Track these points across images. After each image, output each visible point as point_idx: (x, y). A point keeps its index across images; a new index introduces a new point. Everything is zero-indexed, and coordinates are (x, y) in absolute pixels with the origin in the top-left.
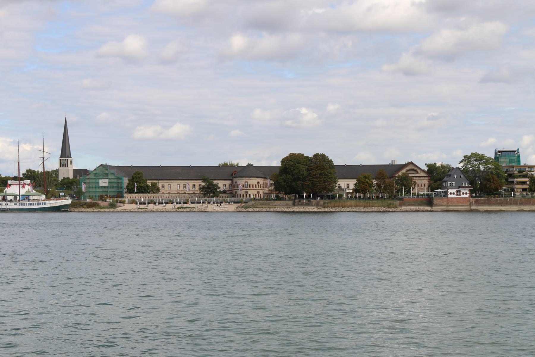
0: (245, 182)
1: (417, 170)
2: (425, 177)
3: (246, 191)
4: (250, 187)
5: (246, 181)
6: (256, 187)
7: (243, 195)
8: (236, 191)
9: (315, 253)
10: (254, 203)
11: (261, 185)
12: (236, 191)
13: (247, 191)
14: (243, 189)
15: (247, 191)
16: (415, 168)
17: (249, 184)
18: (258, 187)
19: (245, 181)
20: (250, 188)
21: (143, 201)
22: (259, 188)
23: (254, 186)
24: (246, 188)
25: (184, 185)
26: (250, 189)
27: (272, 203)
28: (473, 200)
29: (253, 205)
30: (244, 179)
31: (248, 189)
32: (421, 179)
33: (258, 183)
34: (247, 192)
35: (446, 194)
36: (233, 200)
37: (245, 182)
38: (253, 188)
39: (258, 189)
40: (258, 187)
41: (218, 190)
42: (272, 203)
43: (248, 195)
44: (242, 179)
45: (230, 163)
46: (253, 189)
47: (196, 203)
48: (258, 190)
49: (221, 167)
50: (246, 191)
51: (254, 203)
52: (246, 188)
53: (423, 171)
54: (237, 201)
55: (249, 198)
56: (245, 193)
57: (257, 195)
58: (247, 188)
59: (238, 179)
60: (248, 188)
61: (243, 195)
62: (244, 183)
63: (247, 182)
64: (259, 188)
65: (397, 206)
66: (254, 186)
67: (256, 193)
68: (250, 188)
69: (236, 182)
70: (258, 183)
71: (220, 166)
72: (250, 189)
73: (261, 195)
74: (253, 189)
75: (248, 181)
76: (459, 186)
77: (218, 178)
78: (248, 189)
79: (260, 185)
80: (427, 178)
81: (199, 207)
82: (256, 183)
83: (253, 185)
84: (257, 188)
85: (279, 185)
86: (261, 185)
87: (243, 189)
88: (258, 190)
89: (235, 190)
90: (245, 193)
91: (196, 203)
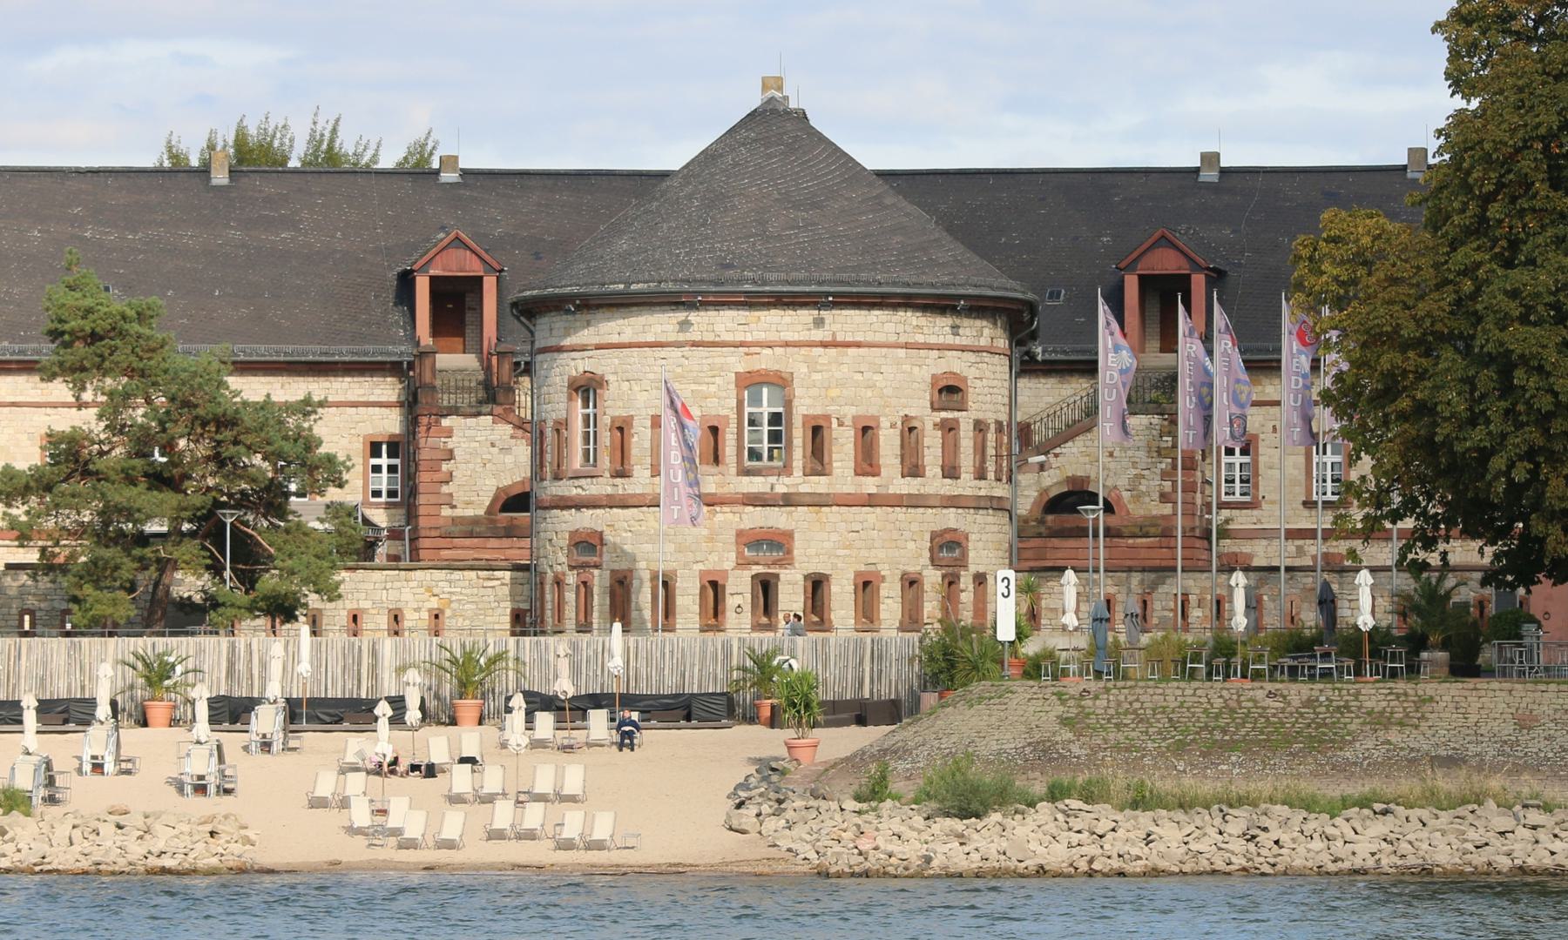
0: (750, 382)
5: (766, 361)
6: (867, 462)
7: (714, 589)
8: (586, 520)
10: (1064, 721)
11: (991, 436)
12: (586, 520)
13: (777, 519)
15: (777, 519)
17: (805, 406)
18: (951, 472)
19: (737, 362)
20: (819, 485)
22: (967, 475)
23: (888, 443)
24: (757, 485)
26: (818, 502)
27: (1380, 721)
29: (1044, 753)
31: (788, 501)
34: (777, 544)
36: (616, 663)
37: (750, 382)
38: (870, 485)
39: (948, 488)
40: (913, 469)
41: (309, 511)
42: (1380, 721)
43: (791, 598)
45: (316, 143)
46: (871, 501)
47: (30, 718)
48: (951, 519)
49: (220, 177)
51: (1064, 721)
52: (757, 485)
53: (454, 411)
54: (669, 686)
56: (742, 564)
57: (932, 578)
58: (782, 486)
60: (798, 482)
61: (714, 589)
63: (781, 382)
64: (967, 475)
66: (888, 443)
67: (915, 556)
68: (819, 485)
69: (587, 388)
70: (950, 392)
71: (204, 171)
74: (871, 501)
75: (795, 364)
76: (1305, 504)
78: (788, 501)
79: (980, 427)
81: (84, 794)
82: (919, 405)
83: (866, 431)
84: (933, 483)
85: (1496, 408)
86: (991, 436)
88: (951, 519)
89: (578, 505)
90: (742, 564)
91: (30, 718)
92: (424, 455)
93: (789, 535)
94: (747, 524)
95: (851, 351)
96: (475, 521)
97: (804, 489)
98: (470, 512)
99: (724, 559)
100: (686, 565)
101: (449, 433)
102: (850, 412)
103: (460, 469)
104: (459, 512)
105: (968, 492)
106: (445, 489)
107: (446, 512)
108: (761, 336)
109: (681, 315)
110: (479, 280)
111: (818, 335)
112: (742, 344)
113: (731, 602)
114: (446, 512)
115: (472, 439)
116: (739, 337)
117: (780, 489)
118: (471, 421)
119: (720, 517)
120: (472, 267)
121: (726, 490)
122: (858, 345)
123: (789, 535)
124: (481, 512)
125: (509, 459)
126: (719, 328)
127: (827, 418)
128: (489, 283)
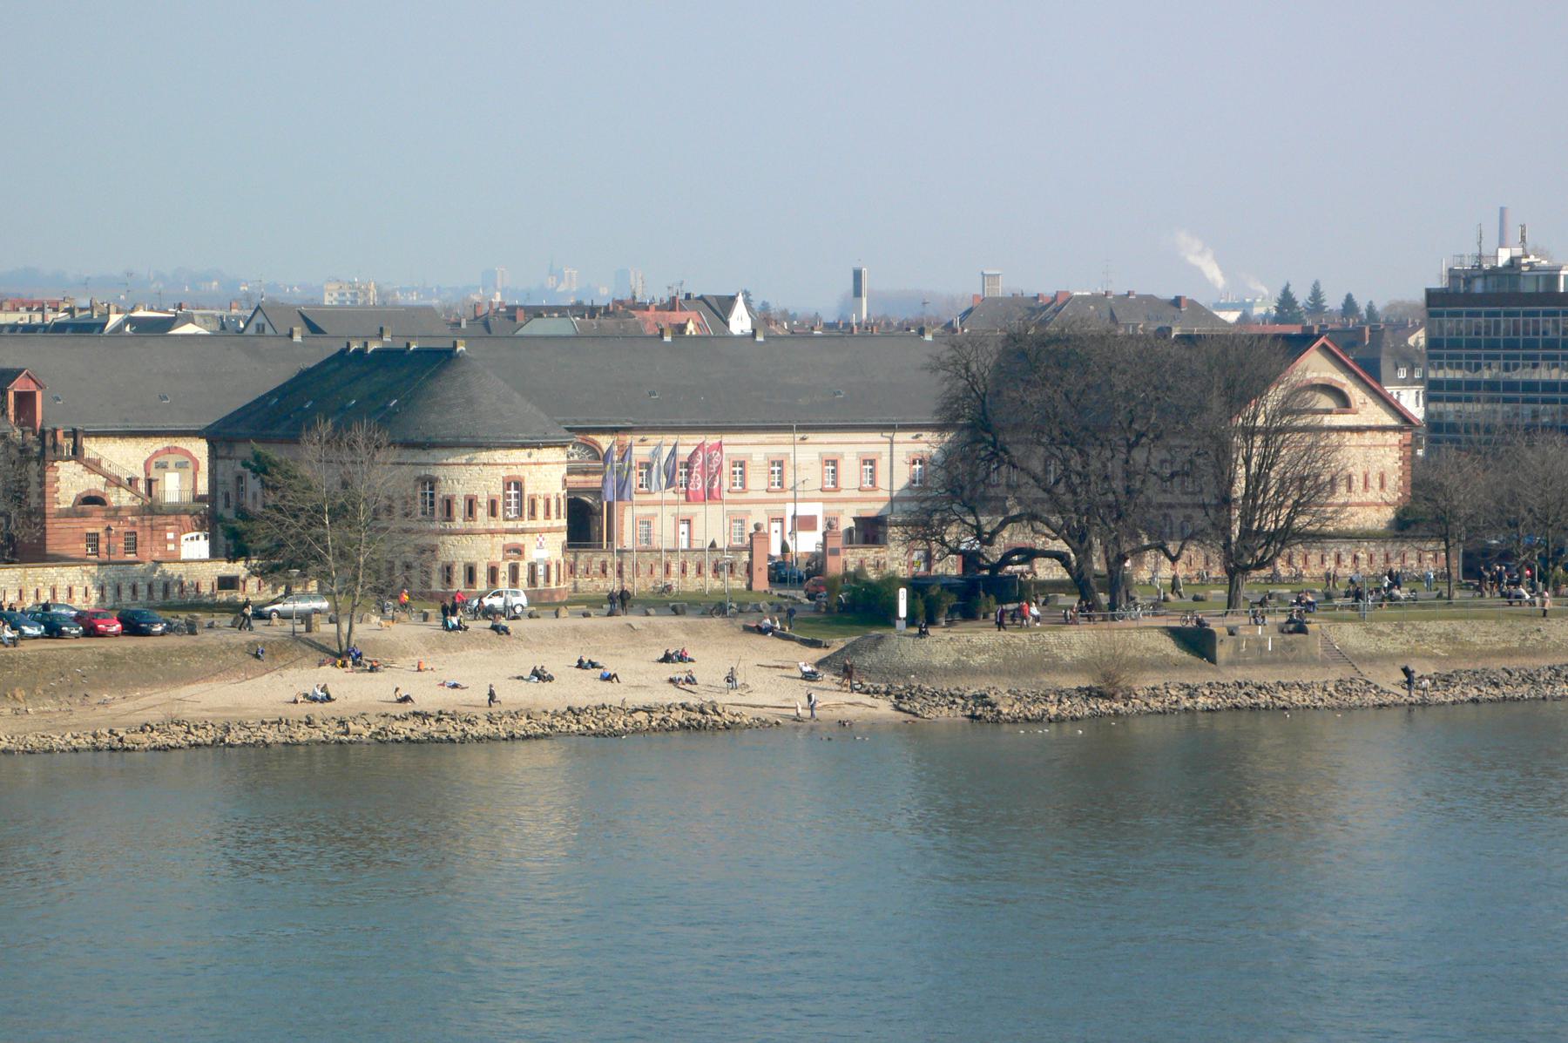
1: (1346, 390)
2: (1384, 429)
3: (511, 539)
4: (449, 514)
5: (514, 472)
9: (1081, 903)
13: (519, 539)
14: (492, 532)
15: (519, 539)
16: (1334, 377)
17: (529, 490)
19: (503, 472)
21: (1223, 592)
25: (156, 468)
26: (532, 532)
28: (936, 571)
30: (499, 455)
31: (523, 532)
32: (1367, 442)
33: (109, 529)
34: (519, 551)
35: (1106, 547)
43: (523, 574)
44: (484, 456)
50: (511, 539)
52: (510, 525)
55: (462, 589)
57: (504, 569)
58: (520, 525)
59: (438, 454)
61: (493, 573)
62: (497, 490)
65: (644, 628)
72: (532, 532)
73: (553, 569)
77: (667, 422)
78: (523, 532)
79: (533, 568)
80: (1393, 438)
87: (492, 532)
92: (48, 480)
93: (523, 546)
94: (507, 542)
95: (544, 466)
96: (68, 509)
97: (528, 526)
98: (66, 506)
99: (498, 557)
100: (481, 560)
101: (57, 469)
102: (543, 492)
103: (62, 485)
104: (61, 506)
105: (542, 526)
106: (56, 495)
107: (56, 506)
108: (512, 461)
109: (528, 450)
110: (33, 394)
111: (533, 460)
112: (505, 464)
113: (501, 575)
114: (56, 506)
115: (67, 472)
116: (504, 461)
117: (520, 527)
118: (66, 463)
119: (496, 539)
120: (32, 387)
121: (498, 527)
122: (545, 464)
123: (523, 546)
124: (70, 505)
125: (82, 481)
126: (496, 457)
127: (536, 495)
128: (39, 395)
